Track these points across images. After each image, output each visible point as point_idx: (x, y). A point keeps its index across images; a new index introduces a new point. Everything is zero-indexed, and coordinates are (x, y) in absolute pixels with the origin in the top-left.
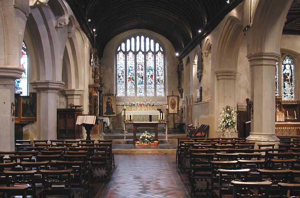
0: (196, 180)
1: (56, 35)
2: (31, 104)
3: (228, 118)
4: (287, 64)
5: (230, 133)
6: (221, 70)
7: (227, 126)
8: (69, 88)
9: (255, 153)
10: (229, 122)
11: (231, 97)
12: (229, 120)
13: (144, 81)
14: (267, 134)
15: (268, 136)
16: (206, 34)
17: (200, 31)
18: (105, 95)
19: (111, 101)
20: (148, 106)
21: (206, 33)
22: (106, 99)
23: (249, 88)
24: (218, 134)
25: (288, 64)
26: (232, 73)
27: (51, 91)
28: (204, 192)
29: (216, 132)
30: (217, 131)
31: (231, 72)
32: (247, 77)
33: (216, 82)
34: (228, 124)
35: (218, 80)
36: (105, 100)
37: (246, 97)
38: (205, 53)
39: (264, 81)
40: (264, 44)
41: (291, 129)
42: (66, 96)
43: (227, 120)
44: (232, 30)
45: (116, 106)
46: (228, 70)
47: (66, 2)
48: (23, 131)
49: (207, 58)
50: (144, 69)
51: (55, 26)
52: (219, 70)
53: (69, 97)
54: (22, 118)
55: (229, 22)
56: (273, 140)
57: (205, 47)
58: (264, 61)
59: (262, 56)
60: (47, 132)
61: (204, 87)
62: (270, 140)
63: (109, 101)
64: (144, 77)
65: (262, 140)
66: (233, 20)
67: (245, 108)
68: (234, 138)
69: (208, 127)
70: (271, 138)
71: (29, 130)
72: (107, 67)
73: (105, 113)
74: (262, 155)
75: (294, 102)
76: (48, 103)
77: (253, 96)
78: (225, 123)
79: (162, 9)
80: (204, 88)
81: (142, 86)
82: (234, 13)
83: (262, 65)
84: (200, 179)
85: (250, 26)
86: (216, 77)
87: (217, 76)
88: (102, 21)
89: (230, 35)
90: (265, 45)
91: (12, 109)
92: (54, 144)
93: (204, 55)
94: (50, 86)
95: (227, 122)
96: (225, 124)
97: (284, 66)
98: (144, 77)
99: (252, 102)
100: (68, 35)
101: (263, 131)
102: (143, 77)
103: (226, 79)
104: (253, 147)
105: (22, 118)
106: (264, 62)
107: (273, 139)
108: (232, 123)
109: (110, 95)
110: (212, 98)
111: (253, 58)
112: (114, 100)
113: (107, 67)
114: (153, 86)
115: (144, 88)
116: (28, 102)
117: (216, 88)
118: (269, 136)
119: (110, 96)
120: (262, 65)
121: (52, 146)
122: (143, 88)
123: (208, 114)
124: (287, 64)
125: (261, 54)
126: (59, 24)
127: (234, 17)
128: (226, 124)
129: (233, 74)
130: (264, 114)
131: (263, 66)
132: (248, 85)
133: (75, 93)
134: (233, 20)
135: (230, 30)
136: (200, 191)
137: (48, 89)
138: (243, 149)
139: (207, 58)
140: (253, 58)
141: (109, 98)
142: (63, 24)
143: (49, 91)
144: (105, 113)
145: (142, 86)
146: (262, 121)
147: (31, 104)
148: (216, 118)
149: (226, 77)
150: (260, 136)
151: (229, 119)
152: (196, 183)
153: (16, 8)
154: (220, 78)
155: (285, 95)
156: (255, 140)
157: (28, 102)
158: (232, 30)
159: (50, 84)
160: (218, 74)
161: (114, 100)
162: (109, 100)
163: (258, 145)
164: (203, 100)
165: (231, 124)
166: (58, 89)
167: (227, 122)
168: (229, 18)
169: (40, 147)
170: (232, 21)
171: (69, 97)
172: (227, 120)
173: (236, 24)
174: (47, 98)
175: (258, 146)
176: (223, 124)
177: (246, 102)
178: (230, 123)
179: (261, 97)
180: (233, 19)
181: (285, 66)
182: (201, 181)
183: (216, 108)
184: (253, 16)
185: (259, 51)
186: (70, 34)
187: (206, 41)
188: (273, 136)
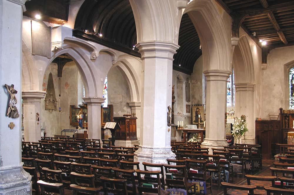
1: (92, 64)
2: (109, 113)
8: (132, 101)
11: (246, 107)
13: (231, 92)
14: (214, 140)
18: (195, 106)
19: (199, 110)
20: (232, 115)
22: (195, 108)
23: (283, 98)
26: (246, 85)
27: (94, 104)
28: (203, 186)
32: (282, 87)
36: (194, 109)
37: (280, 107)
42: (131, 107)
45: (204, 115)
47: (91, 42)
48: (105, 133)
50: (231, 81)
51: (90, 59)
53: (132, 108)
54: (103, 123)
56: (216, 145)
59: (208, 73)
60: (92, 134)
62: (213, 145)
63: (197, 111)
64: (231, 88)
65: (206, 145)
70: (216, 143)
71: (108, 133)
72: (196, 80)
73: (194, 121)
74: (176, 156)
76: (93, 113)
79: (183, 32)
81: (230, 97)
83: (210, 81)
88: (193, 39)
91: (37, 117)
92: (54, 139)
94: (92, 101)
97: (291, 76)
98: (231, 88)
100: (112, 62)
101: (210, 137)
102: (230, 88)
103: (241, 91)
104: (207, 152)
105: (103, 123)
109: (199, 105)
112: (202, 109)
113: (196, 80)
114: (231, 96)
115: (231, 98)
116: (107, 112)
118: (214, 142)
119: (199, 107)
121: (52, 140)
122: (230, 98)
126: (92, 57)
129: (247, 86)
132: (282, 95)
133: (136, 105)
137: (91, 103)
141: (198, 108)
142: (95, 57)
143: (93, 104)
144: (194, 121)
145: (230, 97)
147: (109, 113)
149: (241, 89)
153: (33, 55)
157: (107, 112)
159: (91, 99)
161: (202, 109)
162: (198, 110)
165: (239, 132)
166: (23, 106)
171: (132, 108)
174: (92, 109)
175: (212, 150)
178: (238, 131)
186: (114, 61)
188: (218, 142)
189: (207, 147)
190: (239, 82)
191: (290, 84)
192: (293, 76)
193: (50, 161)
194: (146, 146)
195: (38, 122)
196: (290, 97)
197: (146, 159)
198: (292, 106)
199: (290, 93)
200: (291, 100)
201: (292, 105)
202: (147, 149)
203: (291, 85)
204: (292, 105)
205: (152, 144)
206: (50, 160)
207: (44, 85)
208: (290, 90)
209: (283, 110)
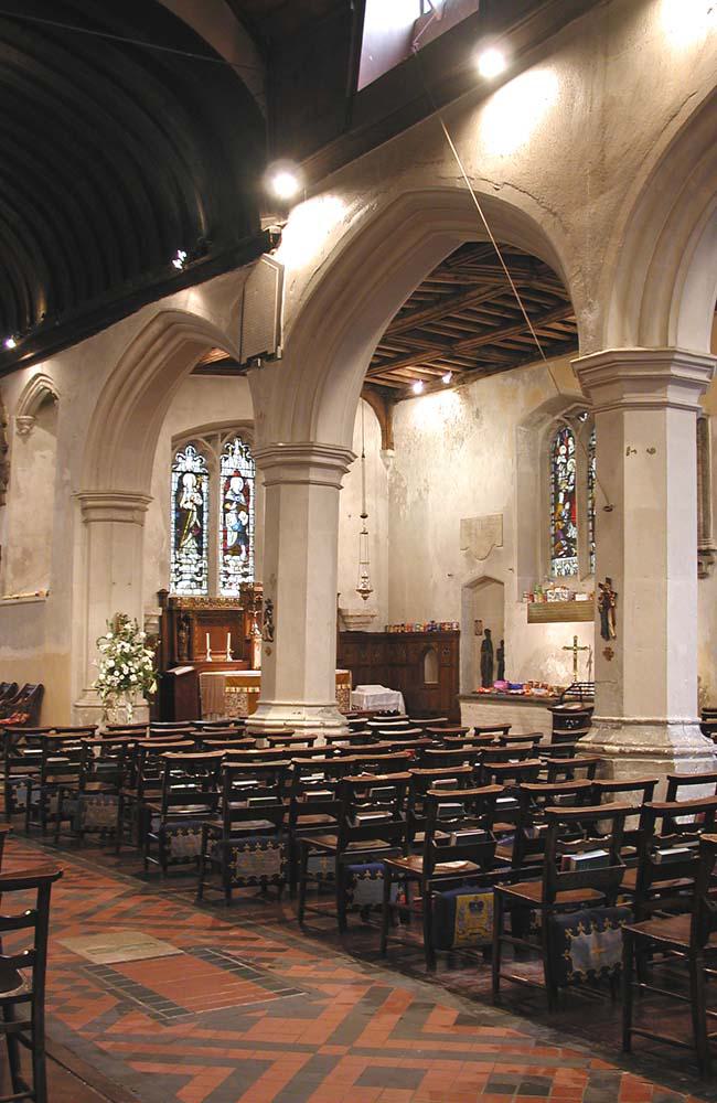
0: (235, 850)
3: (127, 657)
4: (187, 472)
5: (129, 707)
6: (101, 488)
7: (126, 684)
9: (467, 747)
10: (133, 671)
12: (130, 663)
15: (320, 709)
16: (33, 357)
17: (11, 344)
21: (40, 351)
24: (83, 713)
25: (192, 472)
29: (77, 706)
30: (78, 704)
31: (138, 497)
33: (79, 531)
34: (127, 676)
35: (86, 522)
38: (20, 424)
39: (311, 532)
40: (316, 422)
41: (241, 691)
43: (123, 666)
44: (162, 356)
46: (127, 489)
49: (25, 442)
52: (93, 488)
55: (156, 327)
56: (336, 723)
57: (20, 401)
58: (312, 469)
61: (13, 546)
62: (327, 723)
65: (306, 724)
66: (173, 324)
67: (156, 622)
68: (53, 729)
69: (41, 689)
75: (231, 603)
77: (273, 581)
78: (117, 673)
80: (11, 550)
82: (191, 301)
83: (307, 482)
84: (247, 847)
85: (275, 354)
86: (78, 511)
87: (85, 509)
89: (150, 370)
90: (319, 422)
93: (16, 429)
95: (126, 672)
96: (116, 678)
99: (269, 601)
106: (314, 475)
107: (334, 717)
108: (141, 674)
110: (61, 584)
111: (279, 459)
117: (77, 550)
120: (307, 482)
123: (38, 641)
124: (187, 472)
125: (308, 449)
127: (191, 315)
128: (122, 677)
130: (308, 641)
131: (311, 486)
134: (173, 324)
135: (156, 355)
136: (246, 882)
138: (369, 746)
139: (25, 442)
140: (279, 459)
146: (303, 661)
148: (74, 659)
150: (299, 710)
151: (129, 659)
152: (235, 861)
154: (93, 514)
155: (225, 580)
156: (282, 723)
158: (162, 356)
160: (89, 503)
163: (325, 737)
164: (8, 592)
167: (126, 672)
168: (161, 313)
169: (266, 730)
170: (168, 326)
172: (123, 666)
173: (181, 336)
176: (110, 678)
177: (156, 601)
179: (301, 584)
180: (178, 322)
181: (181, 478)
182: (250, 851)
183: (77, 620)
184: (290, 327)
185: (298, 439)
187: (26, 383)
189: (306, 732)
190: (113, 489)
191: (173, 506)
192: (181, 478)
193: (546, 826)
194: (679, 719)
195: (605, 644)
196: (172, 551)
197: (698, 760)
198: (176, 583)
199: (173, 539)
200: (176, 562)
201: (179, 579)
202: (681, 727)
203: (176, 510)
204: (179, 579)
205: (664, 709)
206: (545, 823)
207: (533, 459)
208: (173, 526)
209: (169, 596)
